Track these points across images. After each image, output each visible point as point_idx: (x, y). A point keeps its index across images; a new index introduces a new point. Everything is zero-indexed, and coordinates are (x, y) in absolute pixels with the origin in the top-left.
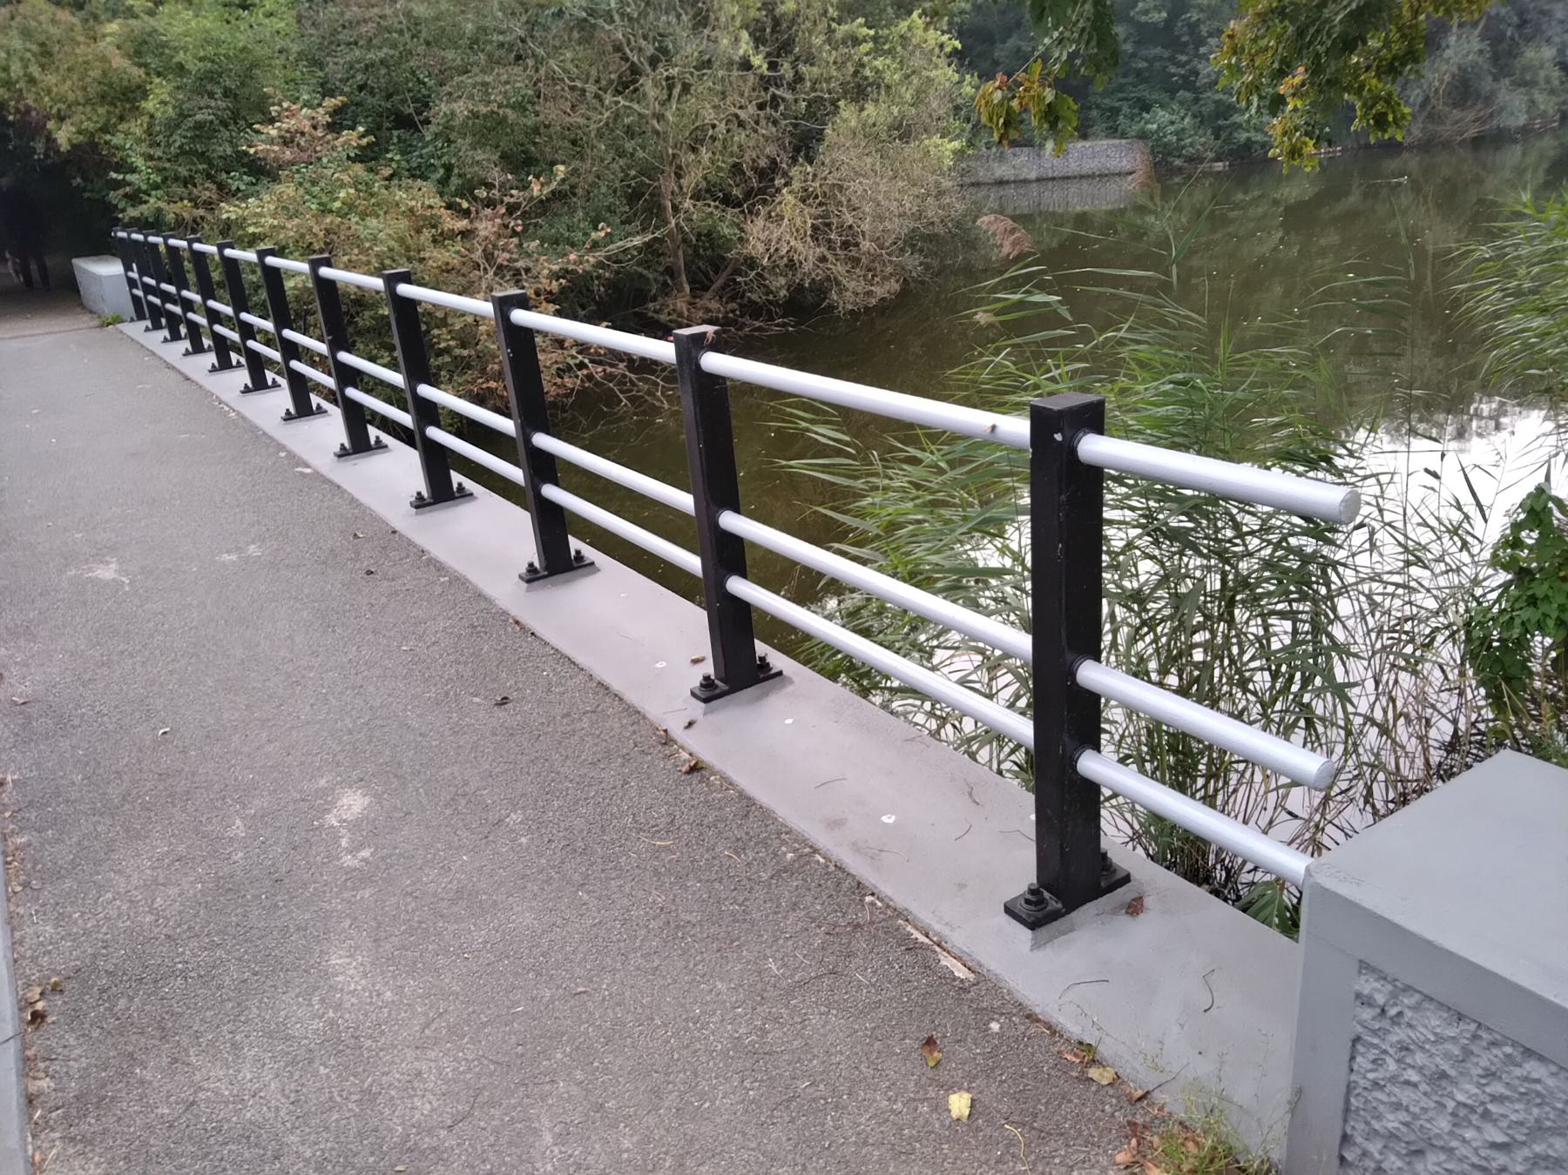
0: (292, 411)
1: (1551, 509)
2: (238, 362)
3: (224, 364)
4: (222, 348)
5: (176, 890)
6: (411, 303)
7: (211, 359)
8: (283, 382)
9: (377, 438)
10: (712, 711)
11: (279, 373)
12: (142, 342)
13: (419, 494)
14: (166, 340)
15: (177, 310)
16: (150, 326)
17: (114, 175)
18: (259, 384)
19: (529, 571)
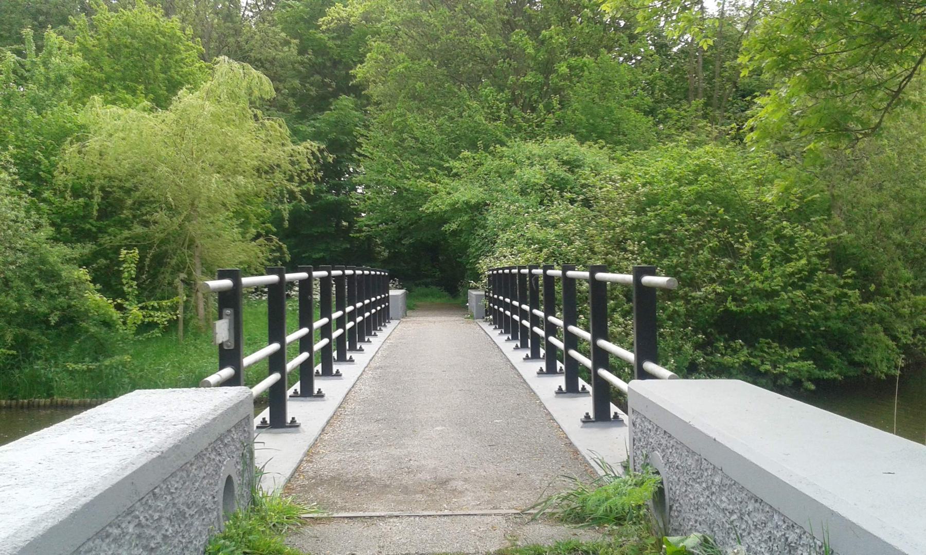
0: (592, 415)
1: (98, 211)
2: (561, 369)
3: (572, 389)
4: (573, 371)
5: (409, 115)
6: (603, 283)
7: (560, 381)
8: (589, 388)
9: (583, 386)
10: (585, 427)
11: (589, 382)
12: (509, 357)
13: (587, 414)
14: (541, 372)
15: (541, 333)
16: (519, 345)
17: (53, 362)
18: (572, 389)
19: (585, 417)
